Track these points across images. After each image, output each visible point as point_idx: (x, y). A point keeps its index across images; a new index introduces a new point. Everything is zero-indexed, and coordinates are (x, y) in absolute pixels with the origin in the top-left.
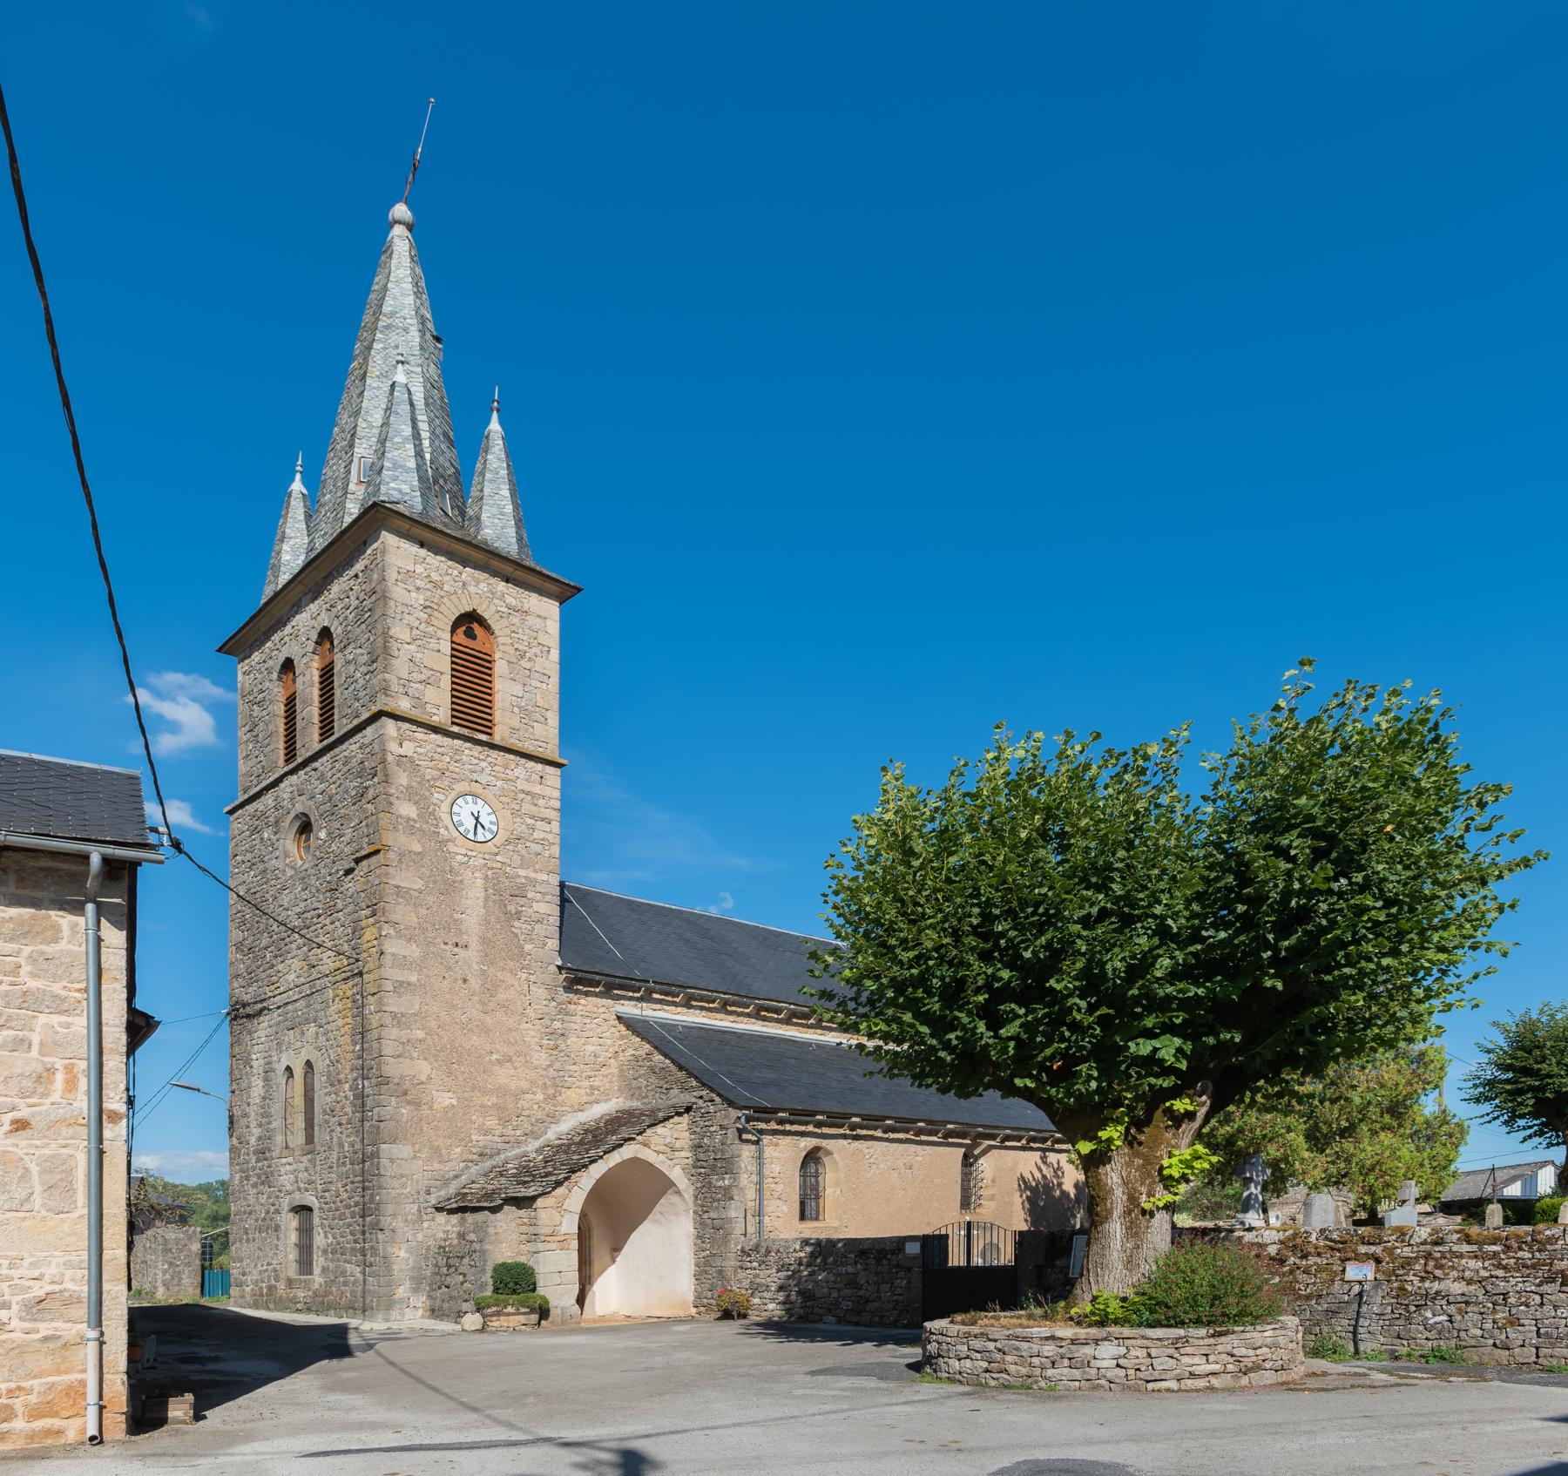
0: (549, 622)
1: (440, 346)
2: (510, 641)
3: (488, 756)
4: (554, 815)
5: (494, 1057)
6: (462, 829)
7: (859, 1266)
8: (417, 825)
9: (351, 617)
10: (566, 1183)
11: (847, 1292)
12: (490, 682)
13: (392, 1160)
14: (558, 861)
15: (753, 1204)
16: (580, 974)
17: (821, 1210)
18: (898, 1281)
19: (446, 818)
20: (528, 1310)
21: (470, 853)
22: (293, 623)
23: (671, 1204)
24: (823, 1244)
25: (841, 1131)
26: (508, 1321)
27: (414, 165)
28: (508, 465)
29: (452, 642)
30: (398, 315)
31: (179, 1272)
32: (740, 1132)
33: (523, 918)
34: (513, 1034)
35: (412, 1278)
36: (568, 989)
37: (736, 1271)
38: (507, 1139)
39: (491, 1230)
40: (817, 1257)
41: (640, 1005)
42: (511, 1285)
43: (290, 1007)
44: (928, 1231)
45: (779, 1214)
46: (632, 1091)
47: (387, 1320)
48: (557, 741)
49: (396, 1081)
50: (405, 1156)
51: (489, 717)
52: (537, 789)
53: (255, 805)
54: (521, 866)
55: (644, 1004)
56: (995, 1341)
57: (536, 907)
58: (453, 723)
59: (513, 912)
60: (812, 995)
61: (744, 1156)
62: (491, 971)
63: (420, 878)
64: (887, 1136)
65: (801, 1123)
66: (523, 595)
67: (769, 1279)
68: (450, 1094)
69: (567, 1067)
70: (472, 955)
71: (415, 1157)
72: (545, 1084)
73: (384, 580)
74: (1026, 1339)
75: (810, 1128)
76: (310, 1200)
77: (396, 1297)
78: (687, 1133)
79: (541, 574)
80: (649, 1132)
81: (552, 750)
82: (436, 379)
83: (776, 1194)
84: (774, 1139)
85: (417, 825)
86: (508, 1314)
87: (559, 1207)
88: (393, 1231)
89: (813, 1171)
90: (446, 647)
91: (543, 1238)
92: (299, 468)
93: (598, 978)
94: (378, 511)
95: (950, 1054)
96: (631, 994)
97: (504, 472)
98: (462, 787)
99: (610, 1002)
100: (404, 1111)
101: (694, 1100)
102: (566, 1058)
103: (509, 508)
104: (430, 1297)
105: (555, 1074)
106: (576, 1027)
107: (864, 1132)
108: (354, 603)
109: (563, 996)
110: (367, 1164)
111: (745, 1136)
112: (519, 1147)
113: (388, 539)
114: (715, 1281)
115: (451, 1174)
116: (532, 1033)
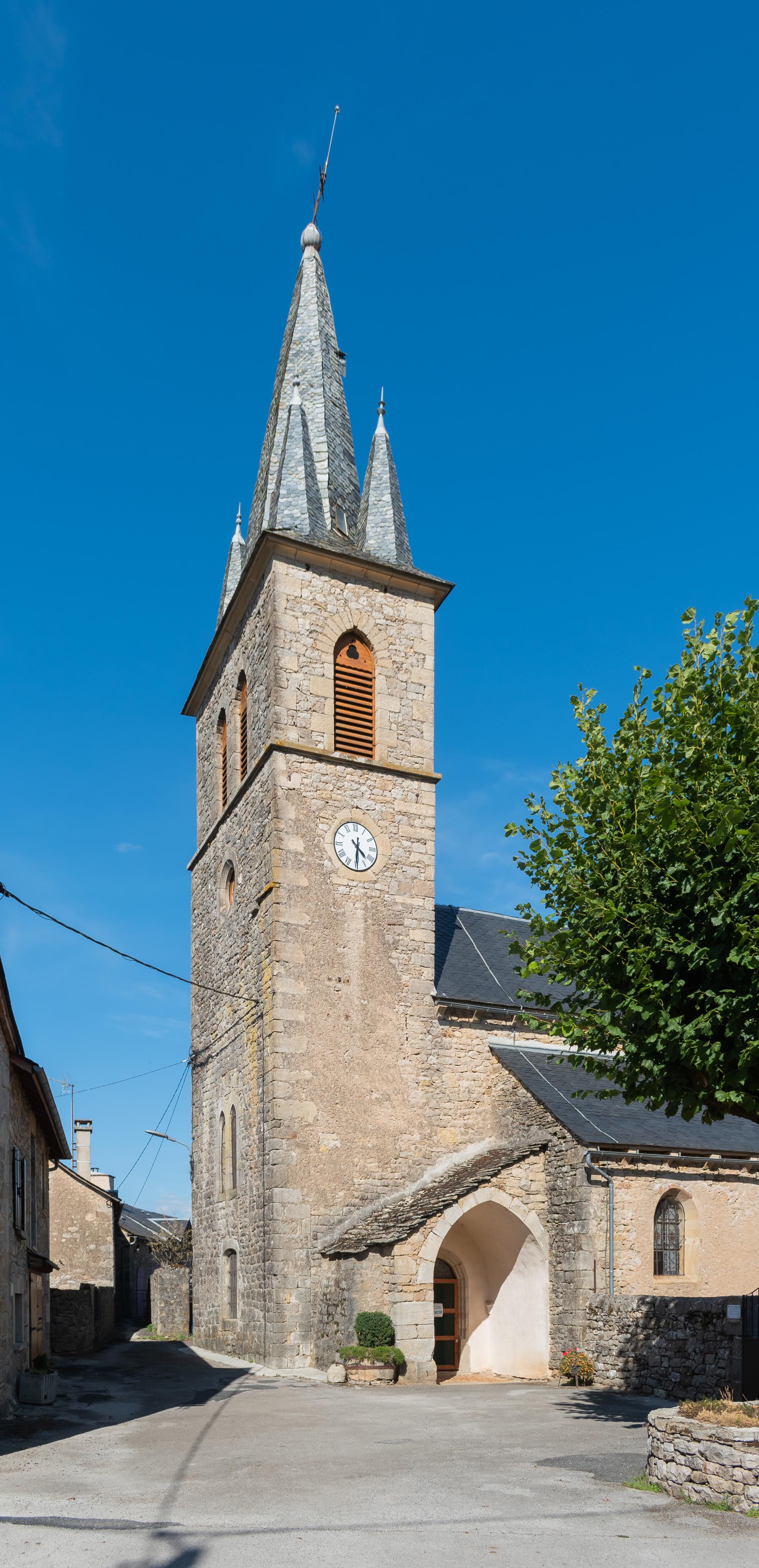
0: (424, 628)
1: (343, 362)
2: (388, 654)
3: (368, 779)
4: (428, 834)
5: (375, 1096)
6: (343, 859)
7: (688, 1330)
8: (304, 859)
9: (256, 655)
10: (422, 1229)
11: (677, 1361)
12: (370, 701)
13: (284, 1205)
14: (433, 884)
15: (603, 1254)
16: (452, 1004)
17: (681, 1262)
18: (722, 1351)
19: (329, 848)
20: (382, 1364)
21: (351, 883)
22: (225, 673)
23: (530, 1253)
24: (657, 1303)
25: (701, 1171)
26: (365, 1375)
27: (322, 180)
28: (391, 468)
29: (336, 664)
30: (305, 340)
31: (173, 1310)
32: (589, 1171)
33: (400, 948)
34: (392, 1071)
35: (301, 1325)
36: (443, 1021)
37: (584, 1331)
38: (386, 1182)
39: (357, 1278)
40: (651, 1318)
41: (512, 1035)
42: (369, 1337)
43: (223, 1053)
44: (747, 1293)
45: (631, 1267)
46: (503, 1131)
47: (280, 1367)
48: (432, 754)
49: (286, 1123)
50: (296, 1201)
52: (413, 808)
53: (201, 862)
54: (398, 893)
55: (517, 1034)
56: (699, 1441)
57: (413, 934)
58: (336, 749)
60: (528, 999)
61: (593, 1200)
63: (306, 913)
64: (753, 1176)
65: (731, 1167)
66: (400, 603)
67: (611, 1342)
68: (334, 1136)
69: (443, 1105)
70: (353, 990)
71: (304, 1201)
72: (421, 1123)
73: (275, 610)
74: (729, 1443)
75: (666, 1167)
76: (235, 1245)
77: (287, 1344)
78: (543, 1174)
79: (415, 577)
80: (504, 1173)
81: (427, 767)
82: (338, 396)
83: (628, 1245)
84: (626, 1180)
85: (304, 859)
86: (365, 1368)
87: (415, 1255)
88: (285, 1276)
89: (672, 1217)
91: (400, 1288)
92: (238, 520)
93: (468, 1006)
95: (656, 1063)
96: (504, 1023)
97: (387, 476)
98: (344, 814)
99: (483, 1032)
100: (294, 1154)
101: (549, 1137)
102: (441, 1095)
103: (390, 513)
104: (316, 1346)
105: (431, 1112)
106: (449, 1060)
107: (727, 1172)
108: (258, 640)
109: (438, 1028)
110: (266, 1208)
111: (594, 1177)
112: (397, 1191)
113: (279, 567)
114: (567, 1340)
115: (337, 1218)
116: (409, 1069)
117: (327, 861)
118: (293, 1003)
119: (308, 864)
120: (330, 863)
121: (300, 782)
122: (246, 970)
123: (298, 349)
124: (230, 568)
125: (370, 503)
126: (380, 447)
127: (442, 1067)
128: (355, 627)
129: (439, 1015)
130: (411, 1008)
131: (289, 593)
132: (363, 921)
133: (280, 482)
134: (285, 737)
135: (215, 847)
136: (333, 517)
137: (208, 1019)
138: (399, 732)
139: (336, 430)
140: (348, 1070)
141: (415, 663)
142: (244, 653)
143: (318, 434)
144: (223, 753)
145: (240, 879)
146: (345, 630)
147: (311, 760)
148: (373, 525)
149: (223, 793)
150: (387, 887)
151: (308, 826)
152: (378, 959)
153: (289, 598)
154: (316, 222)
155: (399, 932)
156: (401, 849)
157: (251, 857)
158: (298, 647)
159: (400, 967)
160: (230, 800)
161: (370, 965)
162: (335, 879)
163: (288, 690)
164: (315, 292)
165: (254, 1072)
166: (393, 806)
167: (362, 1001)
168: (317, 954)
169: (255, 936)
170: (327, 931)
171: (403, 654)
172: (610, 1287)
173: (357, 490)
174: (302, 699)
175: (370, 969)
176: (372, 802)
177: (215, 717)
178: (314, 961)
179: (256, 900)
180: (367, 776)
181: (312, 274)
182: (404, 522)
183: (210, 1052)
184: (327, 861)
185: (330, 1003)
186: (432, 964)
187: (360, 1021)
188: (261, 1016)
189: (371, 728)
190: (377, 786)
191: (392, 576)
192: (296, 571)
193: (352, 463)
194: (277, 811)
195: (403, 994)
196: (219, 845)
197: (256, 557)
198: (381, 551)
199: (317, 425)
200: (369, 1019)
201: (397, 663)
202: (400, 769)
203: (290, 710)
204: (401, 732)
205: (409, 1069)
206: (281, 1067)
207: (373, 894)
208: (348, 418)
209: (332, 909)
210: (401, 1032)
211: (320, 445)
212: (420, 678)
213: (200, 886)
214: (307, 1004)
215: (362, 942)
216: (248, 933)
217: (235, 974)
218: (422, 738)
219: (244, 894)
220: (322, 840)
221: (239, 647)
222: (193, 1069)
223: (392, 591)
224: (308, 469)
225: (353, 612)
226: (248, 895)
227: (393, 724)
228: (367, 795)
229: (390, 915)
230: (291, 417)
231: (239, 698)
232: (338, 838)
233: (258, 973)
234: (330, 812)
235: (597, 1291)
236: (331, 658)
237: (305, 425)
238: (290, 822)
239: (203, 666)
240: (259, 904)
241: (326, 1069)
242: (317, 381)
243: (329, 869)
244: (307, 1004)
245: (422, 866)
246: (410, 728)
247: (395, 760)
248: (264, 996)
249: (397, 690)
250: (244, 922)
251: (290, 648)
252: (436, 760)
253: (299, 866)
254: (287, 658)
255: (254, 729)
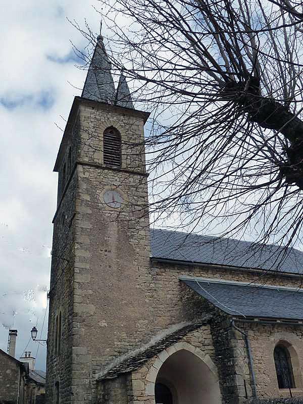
13: (77, 355)
63: (91, 224)
70: (113, 255)
83: (262, 371)
87: (144, 378)
113: (82, 108)
128: (112, 126)
172: (254, 395)
235: (249, 398)
253: (87, 205)
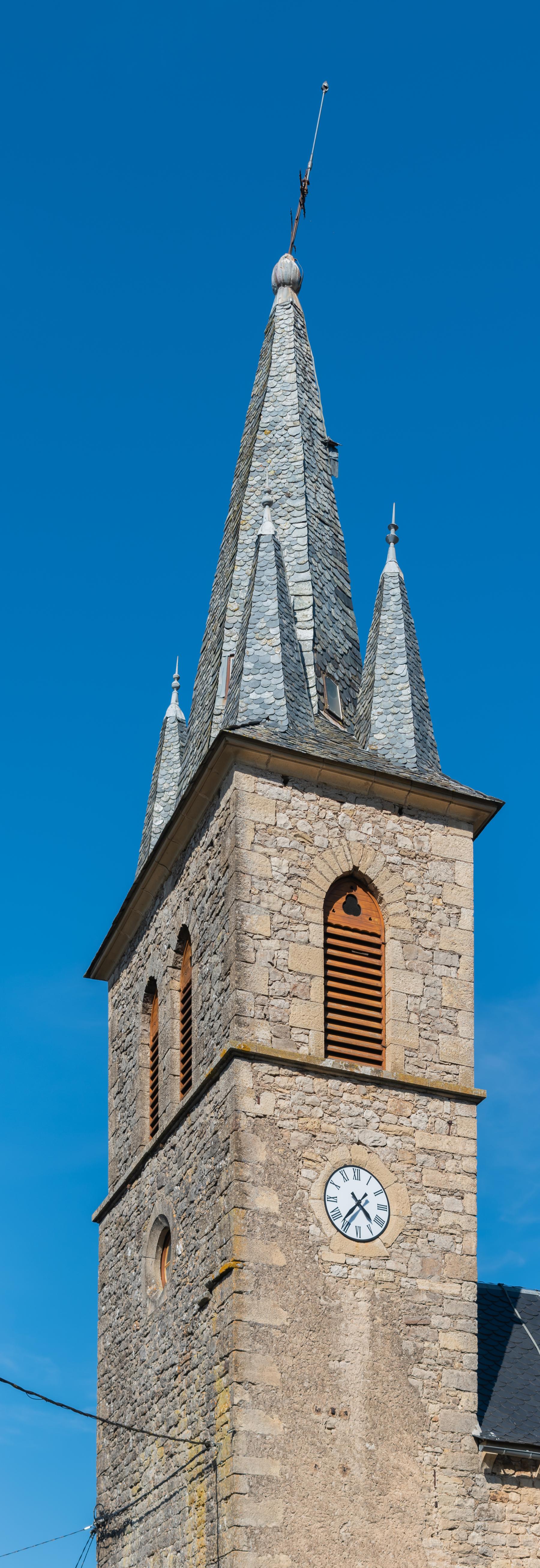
0: (459, 866)
1: (334, 455)
2: (405, 908)
3: (375, 1099)
4: (467, 1183)
8: (279, 1224)
9: (207, 906)
12: (379, 978)
14: (474, 1260)
16: (505, 1450)
19: (316, 1206)
21: (350, 1261)
22: (156, 925)
28: (408, 624)
29: (326, 924)
33: (426, 1361)
34: (413, 1555)
36: (492, 1475)
43: (151, 1520)
51: (377, 1036)
52: (443, 1143)
54: (422, 1275)
58: (328, 1053)
59: (411, 1351)
62: (381, 1452)
63: (283, 1307)
66: (422, 831)
73: (236, 846)
81: (466, 1083)
82: (328, 507)
85: (279, 1224)
90: (317, 934)
92: (175, 683)
94: (227, 743)
97: (401, 638)
98: (339, 1154)
106: (501, 1539)
108: (210, 885)
109: (484, 1487)
113: (243, 781)
117: (313, 1226)
118: (262, 1448)
119: (286, 1231)
120: (318, 1230)
121: (273, 1105)
122: (189, 1392)
123: (268, 439)
124: (163, 757)
125: (377, 677)
126: (391, 592)
127: (490, 1550)
128: (355, 868)
129: (486, 1466)
130: (442, 1456)
131: (257, 820)
132: (368, 1319)
133: (243, 650)
134: (252, 1038)
135: (140, 1192)
136: (319, 693)
137: (125, 1462)
138: (421, 1025)
139: (324, 560)
140: (345, 1554)
141: (445, 920)
142: (188, 900)
143: (298, 568)
144: (151, 1044)
145: (179, 1247)
146: (340, 873)
147: (290, 1072)
148: (380, 710)
149: (152, 1106)
150: (404, 1266)
151: (285, 1172)
152: (391, 1378)
153: (258, 826)
154: (294, 250)
155: (423, 1335)
156: (425, 1207)
157: (197, 1216)
158: (271, 902)
159: (426, 1391)
160: (164, 1123)
161: (380, 1388)
162: (326, 1254)
163: (256, 966)
164: (292, 356)
165: (201, 1554)
166: (413, 1140)
167: (368, 1445)
168: (299, 1372)
169: (204, 1339)
170: (315, 1335)
171: (427, 907)
173: (356, 647)
174: (278, 978)
175: (379, 1394)
176: (381, 1134)
177: (140, 988)
178: (295, 1383)
179: (207, 1286)
180: (374, 1094)
181: (288, 329)
182: (428, 704)
183: (128, 1516)
184: (313, 1226)
185: (318, 1448)
186: (475, 1386)
187: (364, 1476)
188: (214, 1466)
189: (379, 1020)
190: (389, 1109)
191: (409, 791)
192: (268, 786)
193: (348, 607)
194: (239, 1150)
195: (431, 1434)
196: (146, 1191)
197: (209, 766)
198: (394, 751)
199: (296, 554)
200: (378, 1473)
201: (418, 921)
202: (424, 1084)
203: (258, 995)
204: (425, 1026)
205: (440, 1553)
206: (245, 1548)
207: (384, 1277)
208: (342, 538)
209: (322, 1301)
210: (427, 1494)
211: (301, 585)
212: (453, 943)
213: (114, 1249)
214: (284, 1450)
215: (367, 1352)
216: (192, 1334)
217: (171, 1395)
218: (456, 1034)
219: (187, 1272)
220: (306, 1194)
221: (178, 888)
222: (100, 1540)
223: (411, 812)
224: (285, 630)
225: (352, 845)
226: (193, 1274)
227: (412, 1015)
228: (374, 1124)
229: (409, 1310)
230: (260, 554)
231: (179, 965)
232: (331, 1191)
233: (209, 1399)
234: (318, 1151)
236: (319, 916)
237: (280, 565)
238: (259, 1166)
239: (123, 910)
240: (211, 1290)
241: (312, 1552)
242: (297, 489)
243: (318, 1239)
244: (284, 1450)
245: (458, 1233)
246: (438, 1020)
247: (416, 1070)
248: (218, 1436)
249: (418, 962)
250: (185, 1315)
251: (259, 903)
252: (477, 1068)
253: (272, 1234)
254: (255, 917)
255: (203, 1019)
